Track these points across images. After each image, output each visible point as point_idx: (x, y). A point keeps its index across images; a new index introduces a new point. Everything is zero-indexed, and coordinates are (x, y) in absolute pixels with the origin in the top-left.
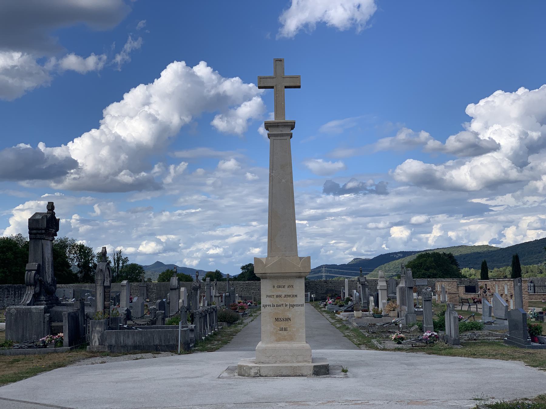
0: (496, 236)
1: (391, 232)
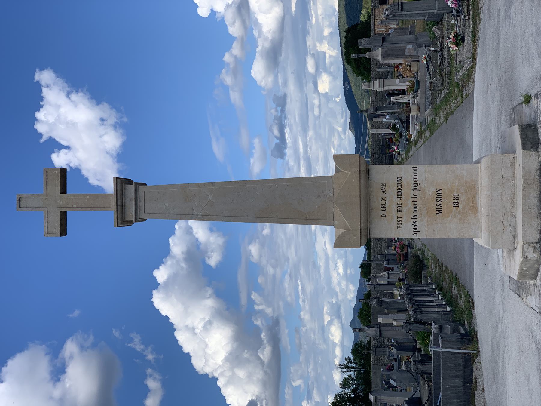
1: (323, 92)
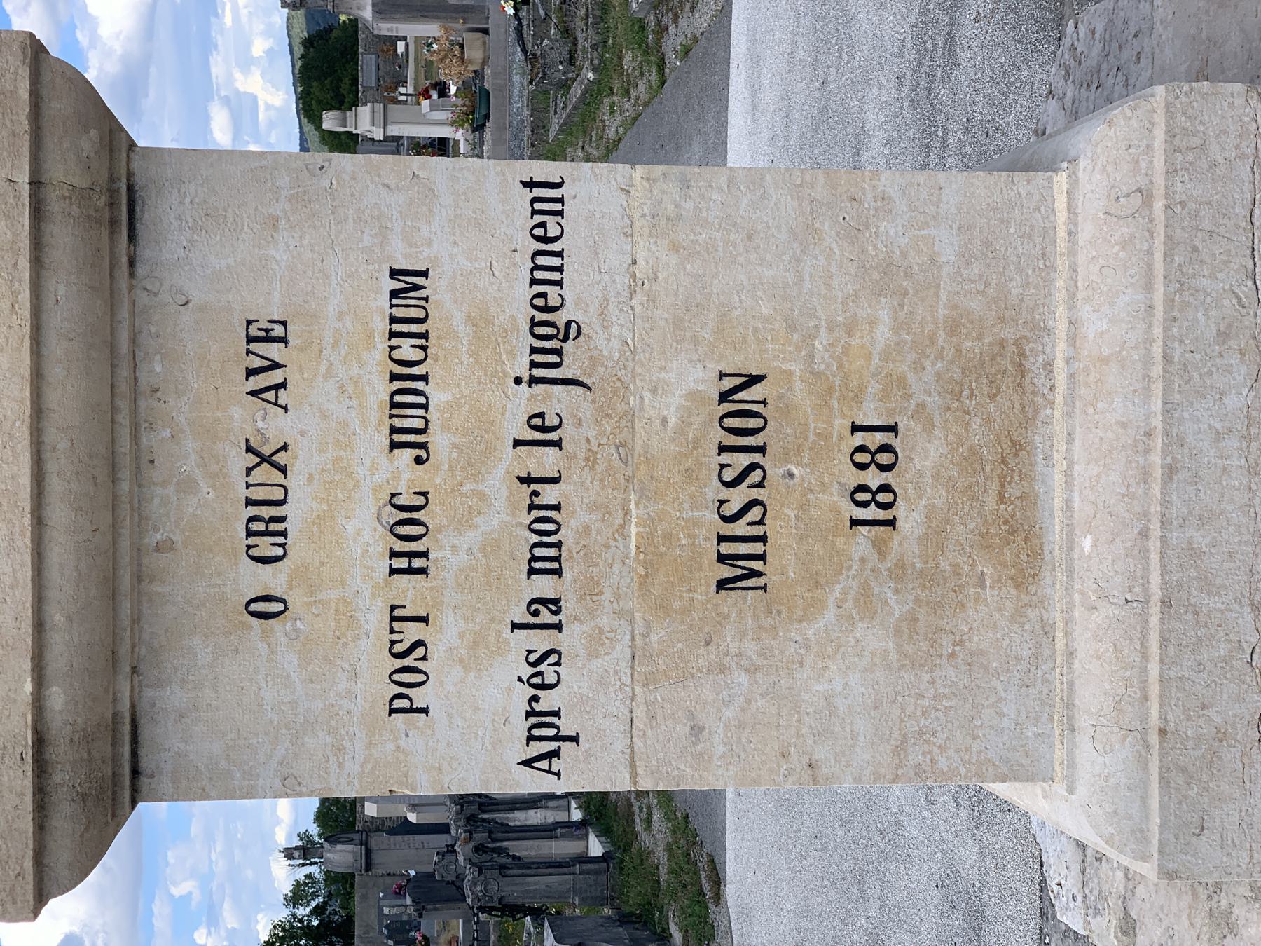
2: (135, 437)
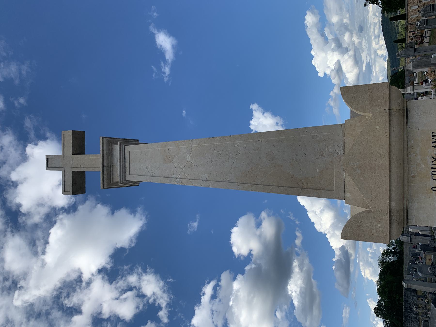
0: (382, 58)
2: (408, 156)
